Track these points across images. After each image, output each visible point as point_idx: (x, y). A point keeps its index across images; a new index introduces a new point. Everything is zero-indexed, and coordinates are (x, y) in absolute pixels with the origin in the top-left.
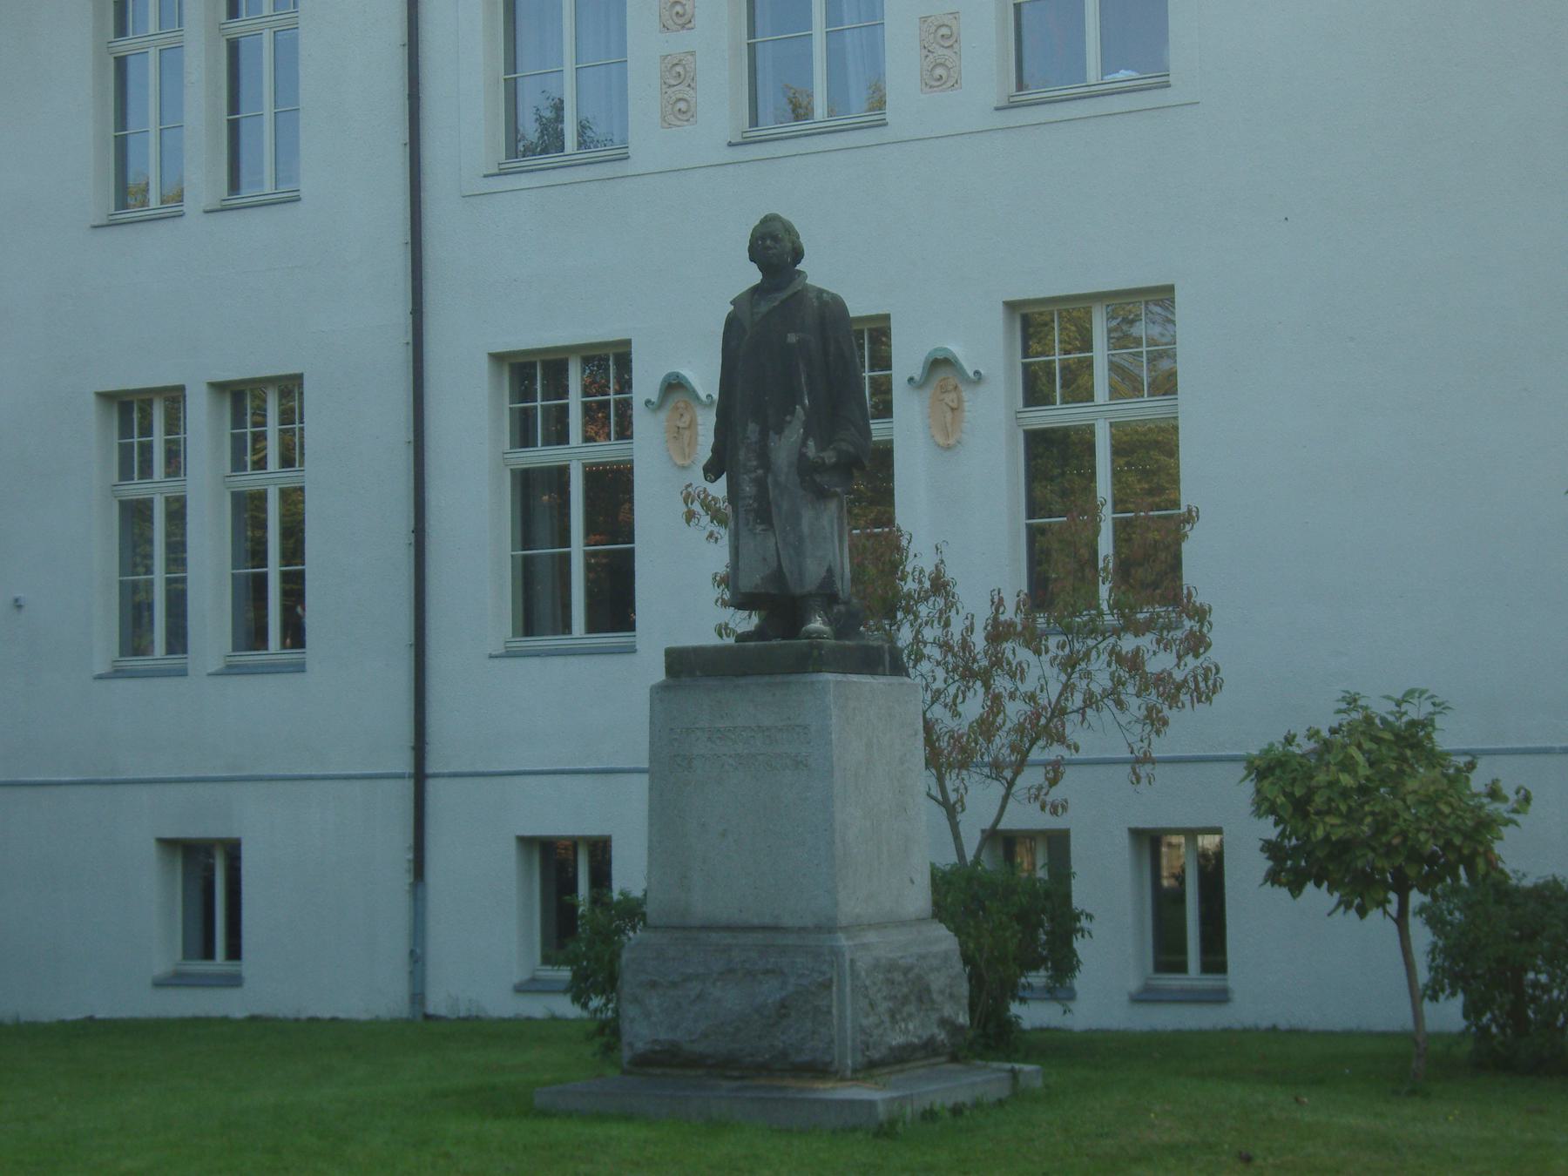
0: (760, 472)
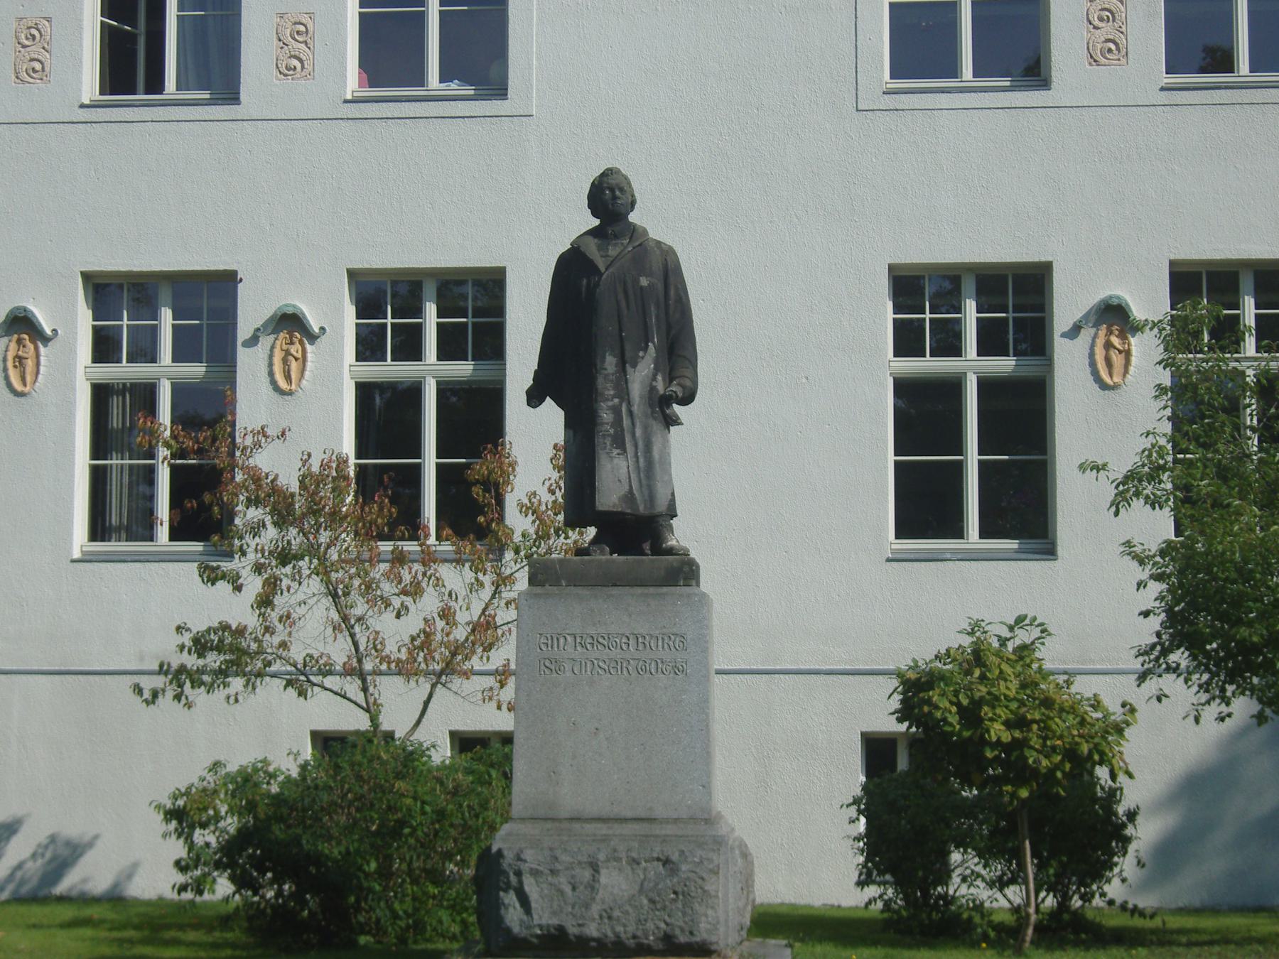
0: (616, 400)
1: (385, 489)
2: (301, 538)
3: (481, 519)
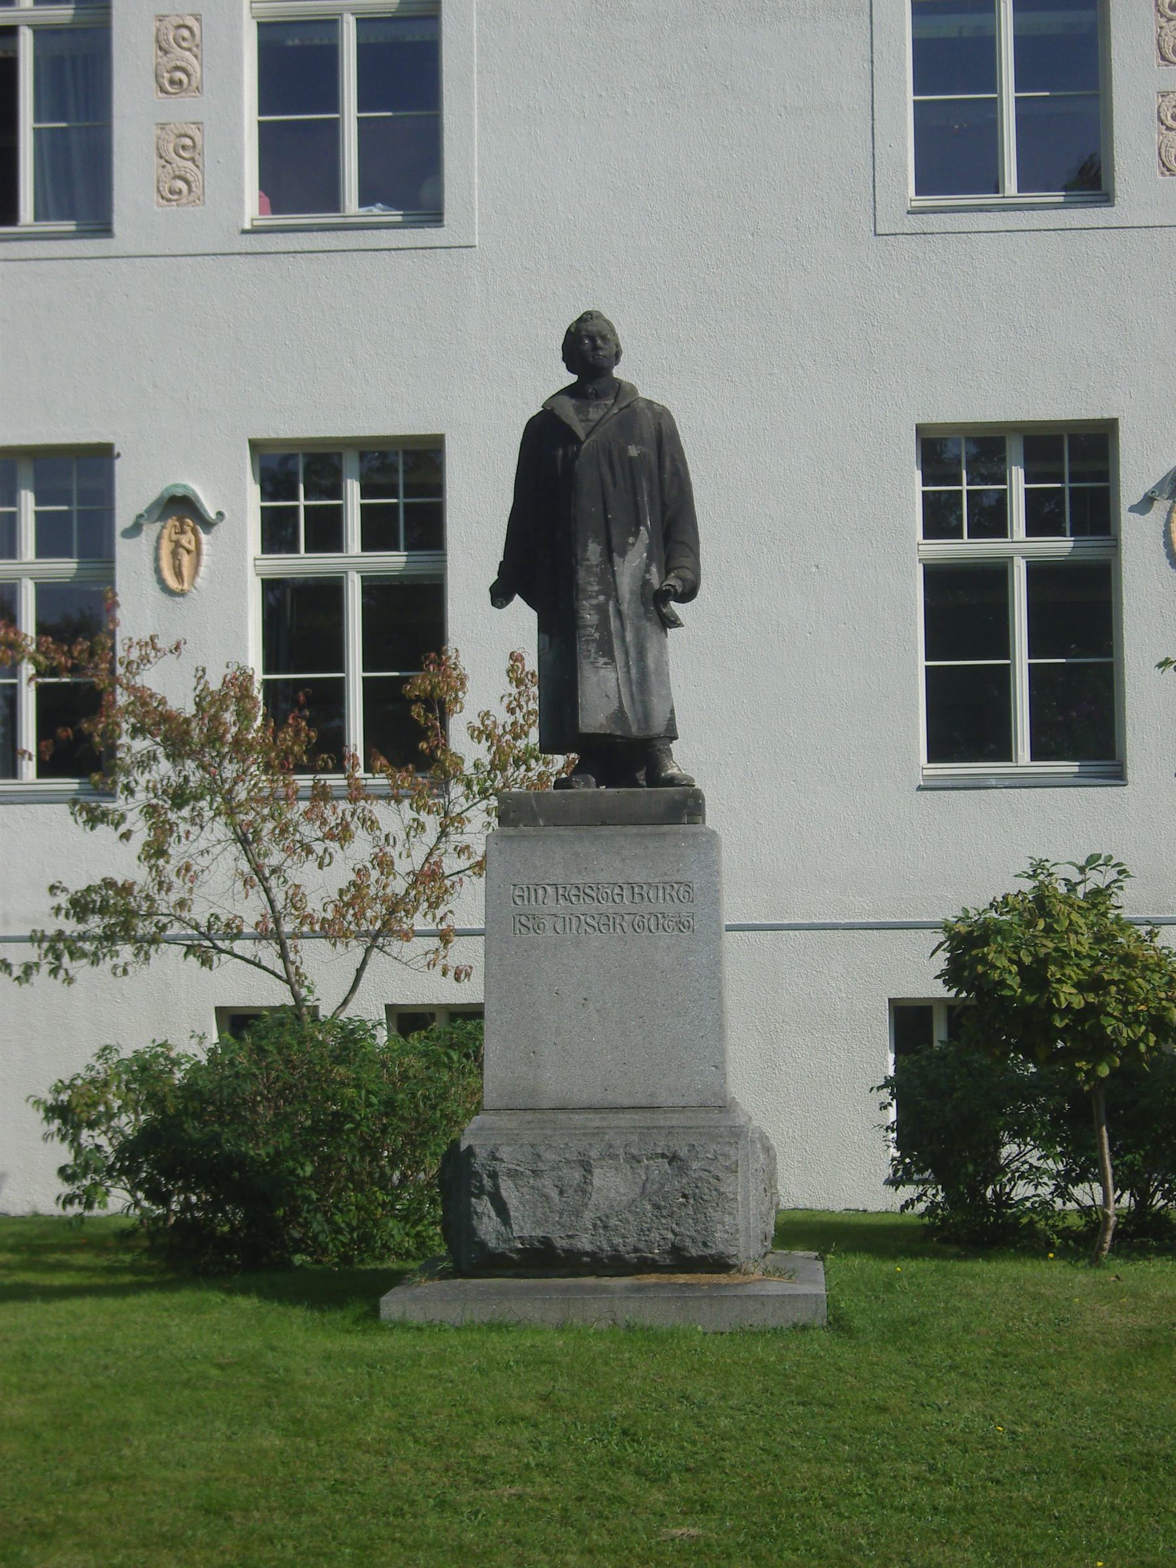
0: (602, 598)
1: (301, 709)
2: (200, 774)
3: (423, 745)
